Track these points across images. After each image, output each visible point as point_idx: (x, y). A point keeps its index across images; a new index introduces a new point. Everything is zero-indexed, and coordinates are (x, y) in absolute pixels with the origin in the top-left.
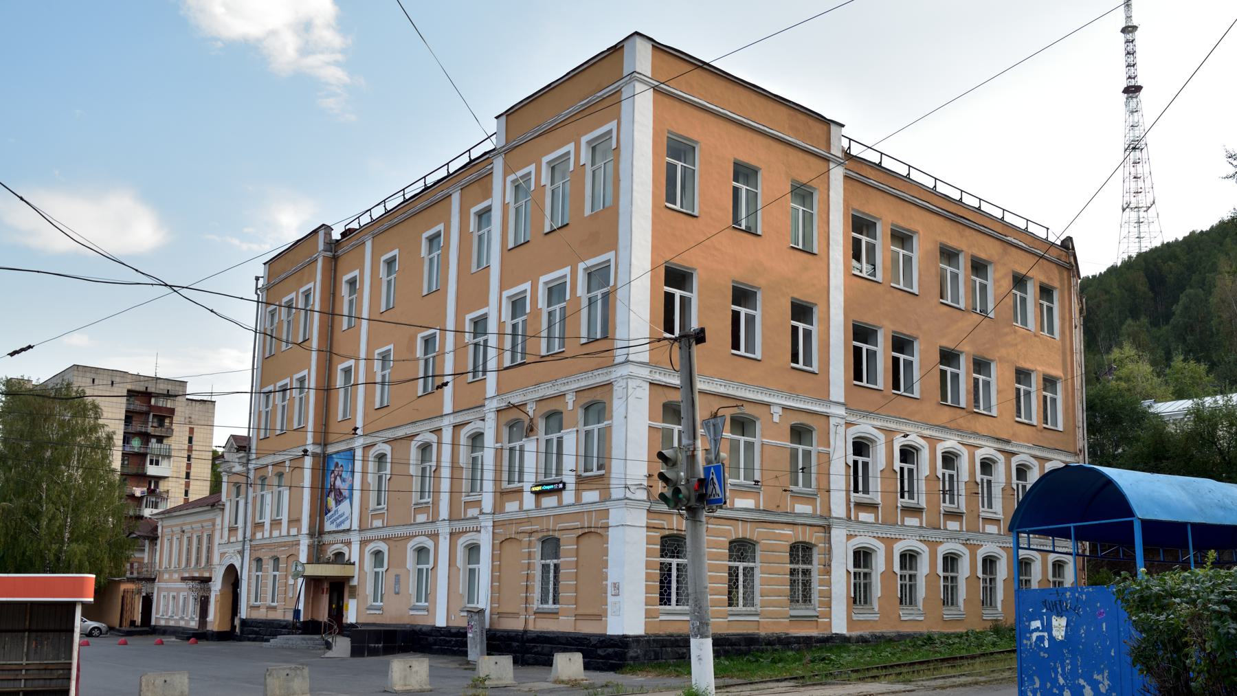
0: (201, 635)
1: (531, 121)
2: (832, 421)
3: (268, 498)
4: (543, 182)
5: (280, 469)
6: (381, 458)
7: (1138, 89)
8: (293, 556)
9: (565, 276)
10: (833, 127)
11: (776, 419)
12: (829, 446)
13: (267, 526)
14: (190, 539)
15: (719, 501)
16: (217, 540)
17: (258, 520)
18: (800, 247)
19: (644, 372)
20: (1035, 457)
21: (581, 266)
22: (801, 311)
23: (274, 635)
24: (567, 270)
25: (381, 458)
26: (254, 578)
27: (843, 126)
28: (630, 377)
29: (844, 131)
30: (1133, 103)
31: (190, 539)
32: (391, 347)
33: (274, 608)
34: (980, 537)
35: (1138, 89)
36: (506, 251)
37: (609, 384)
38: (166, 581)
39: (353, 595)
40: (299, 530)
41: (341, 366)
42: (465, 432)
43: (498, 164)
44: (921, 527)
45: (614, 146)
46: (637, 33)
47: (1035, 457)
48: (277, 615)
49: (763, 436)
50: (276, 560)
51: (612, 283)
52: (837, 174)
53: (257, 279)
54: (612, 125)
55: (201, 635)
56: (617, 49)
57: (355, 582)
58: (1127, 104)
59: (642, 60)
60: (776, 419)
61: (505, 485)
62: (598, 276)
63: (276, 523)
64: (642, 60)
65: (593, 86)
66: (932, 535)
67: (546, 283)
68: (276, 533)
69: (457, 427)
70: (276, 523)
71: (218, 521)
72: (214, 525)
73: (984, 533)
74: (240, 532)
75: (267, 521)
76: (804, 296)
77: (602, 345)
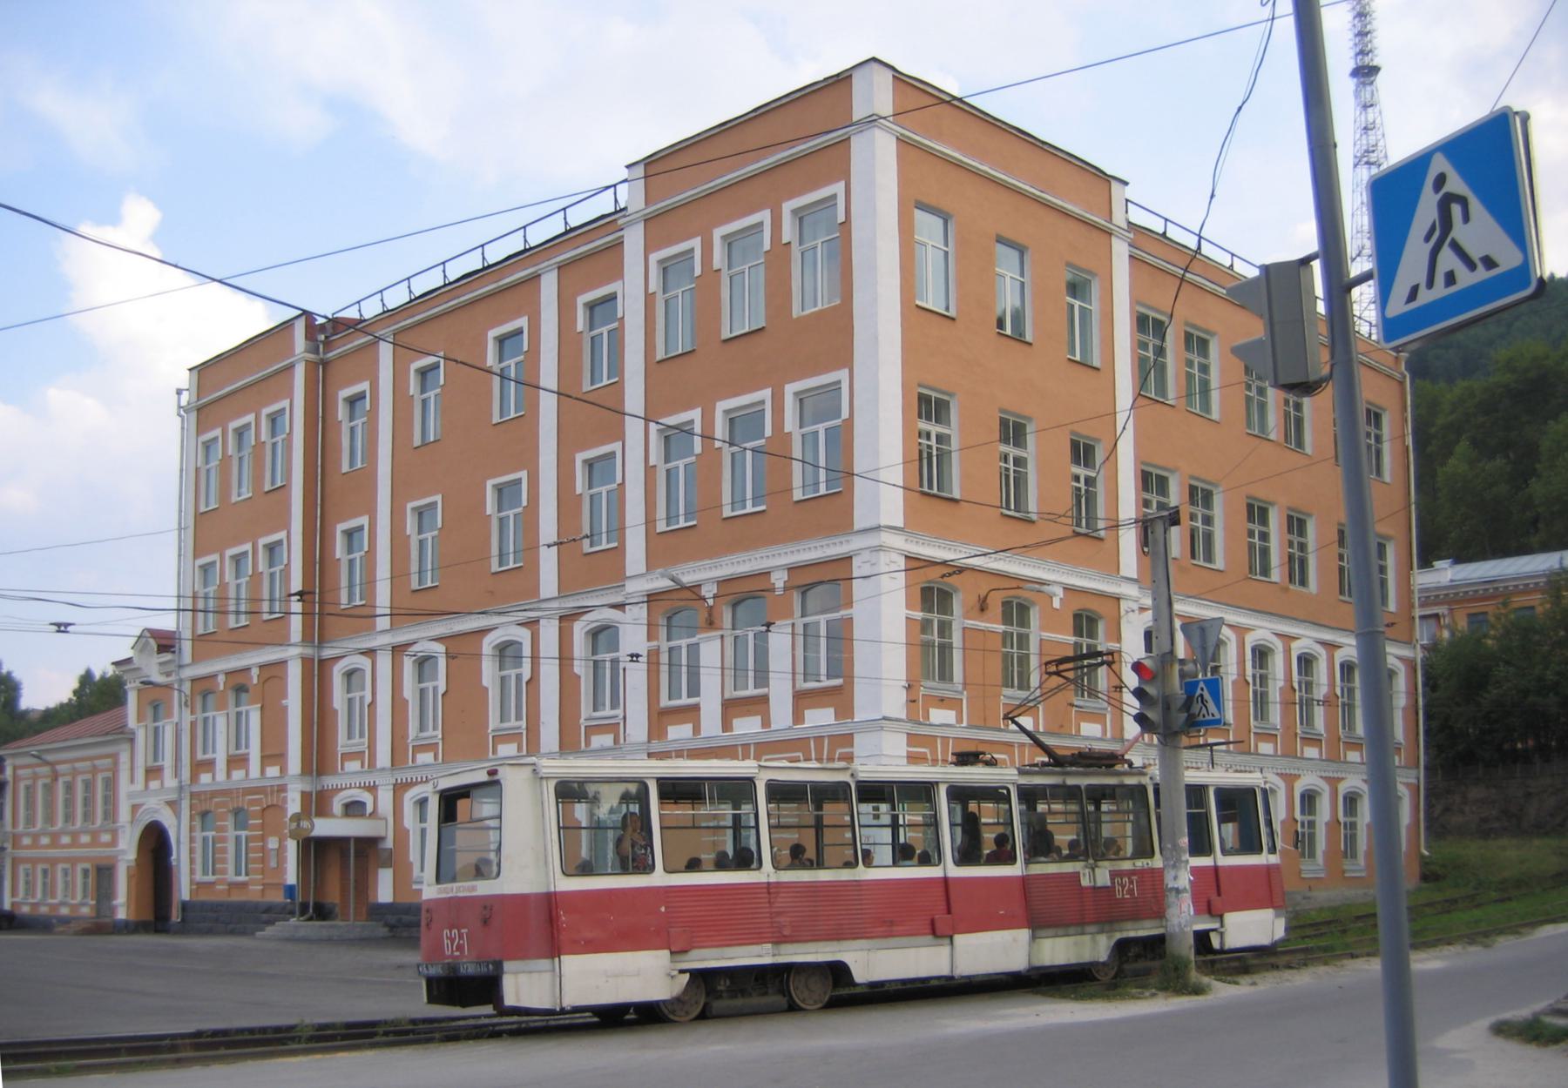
0: (102, 927)
1: (700, 177)
2: (1124, 605)
3: (221, 722)
4: (717, 264)
5: (240, 680)
6: (423, 662)
7: (1374, 70)
8: (280, 808)
9: (763, 402)
10: (1114, 185)
11: (1056, 604)
12: (1119, 639)
13: (221, 765)
14: (70, 788)
15: (1218, 722)
16: (124, 787)
17: (200, 756)
18: (1078, 358)
19: (898, 541)
20: (1323, 643)
21: (790, 389)
22: (1082, 452)
23: (270, 922)
24: (766, 394)
25: (423, 662)
26: (198, 846)
27: (1126, 183)
28: (879, 549)
29: (1129, 192)
30: (1366, 94)
31: (70, 788)
32: (438, 498)
33: (244, 885)
34: (1298, 763)
35: (1374, 70)
36: (653, 367)
37: (847, 560)
38: (27, 847)
39: (387, 863)
40: (283, 770)
41: (341, 527)
42: (579, 629)
43: (1158, 342)
44: (1275, 755)
45: (841, 218)
46: (874, 59)
47: (1323, 643)
48: (254, 893)
49: (1043, 628)
50: (237, 812)
51: (845, 414)
52: (1121, 250)
53: (179, 392)
54: (838, 188)
55: (102, 927)
56: (841, 81)
57: (389, 844)
58: (1357, 94)
59: (875, 97)
60: (1056, 604)
61: (665, 702)
62: (821, 404)
63: (237, 761)
64: (875, 97)
65: (802, 132)
66: (1286, 766)
67: (727, 412)
68: (238, 775)
69: (567, 619)
70: (237, 761)
71: (124, 758)
72: (116, 764)
73: (1346, 762)
74: (168, 772)
75: (221, 759)
76: (1086, 431)
77: (834, 508)
